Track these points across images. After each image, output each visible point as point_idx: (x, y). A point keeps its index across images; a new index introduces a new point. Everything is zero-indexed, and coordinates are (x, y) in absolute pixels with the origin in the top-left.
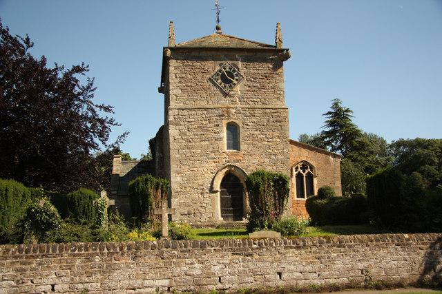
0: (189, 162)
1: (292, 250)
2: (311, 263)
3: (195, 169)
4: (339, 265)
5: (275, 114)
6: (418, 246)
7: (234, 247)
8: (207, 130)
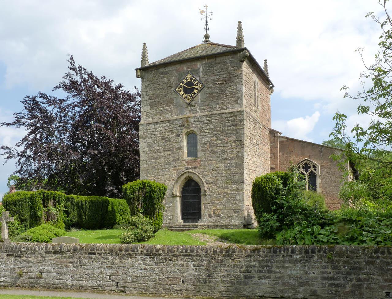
0: (154, 171)
1: (51, 255)
2: (66, 266)
3: (160, 177)
4: (89, 269)
5: (231, 119)
6: (168, 258)
7: (8, 249)
8: (169, 141)
